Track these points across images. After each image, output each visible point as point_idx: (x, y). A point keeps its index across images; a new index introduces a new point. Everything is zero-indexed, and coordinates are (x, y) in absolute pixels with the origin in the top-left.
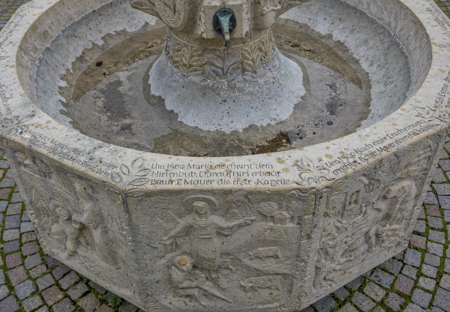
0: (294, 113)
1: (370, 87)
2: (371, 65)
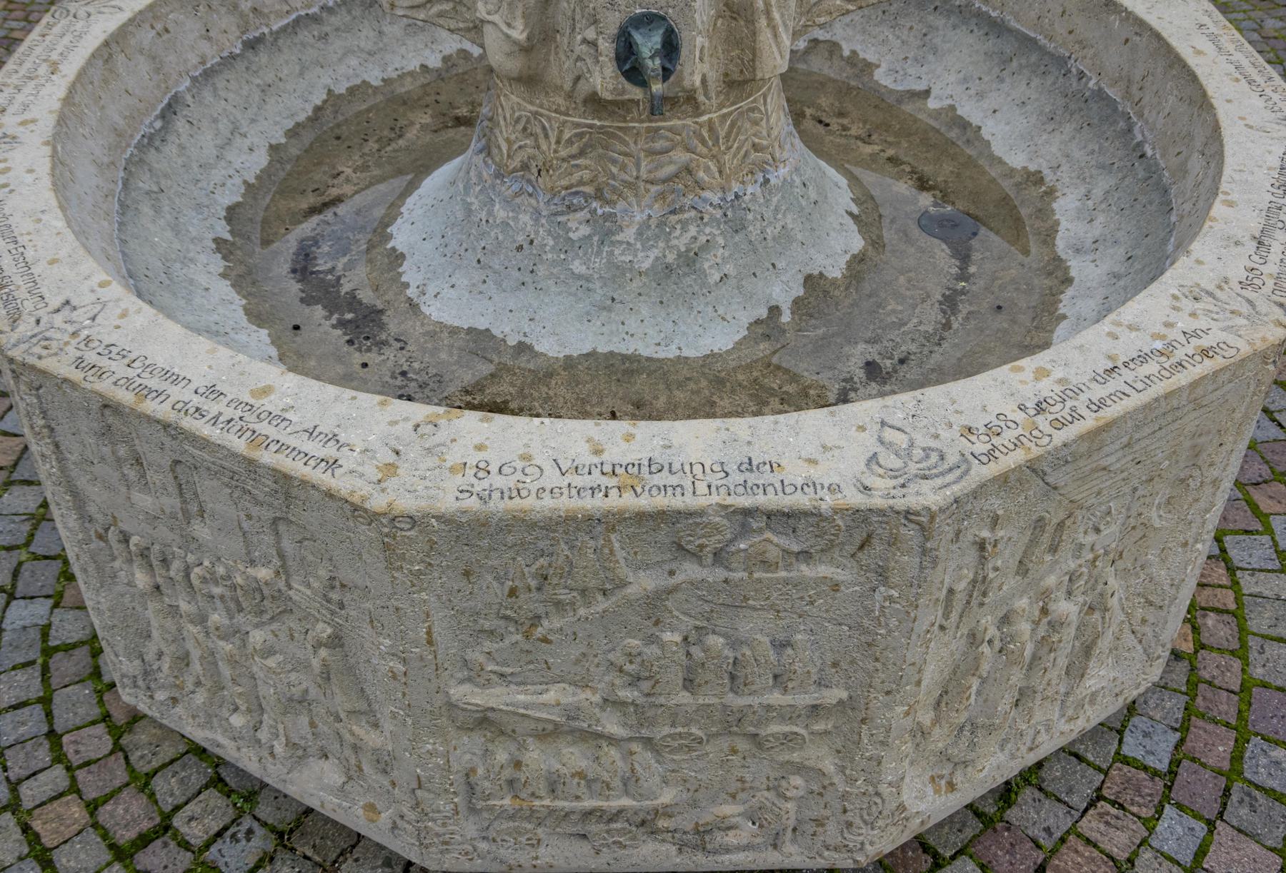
0: (454, 331)
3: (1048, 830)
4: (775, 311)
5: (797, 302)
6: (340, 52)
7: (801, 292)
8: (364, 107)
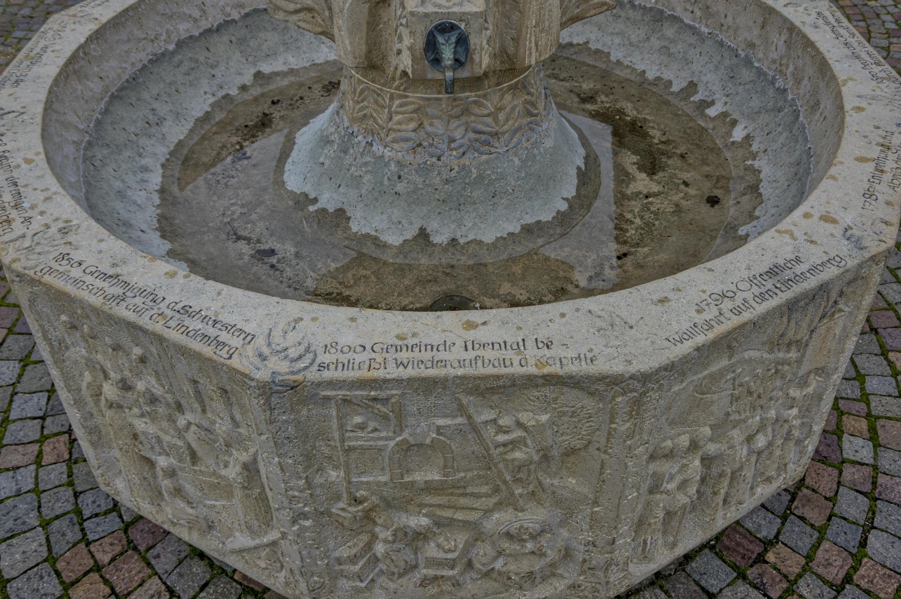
1: (180, 144)
2: (145, 169)
3: (158, 556)
4: (315, 200)
5: (324, 210)
6: (617, 30)
7: (331, 210)
8: (591, 63)
